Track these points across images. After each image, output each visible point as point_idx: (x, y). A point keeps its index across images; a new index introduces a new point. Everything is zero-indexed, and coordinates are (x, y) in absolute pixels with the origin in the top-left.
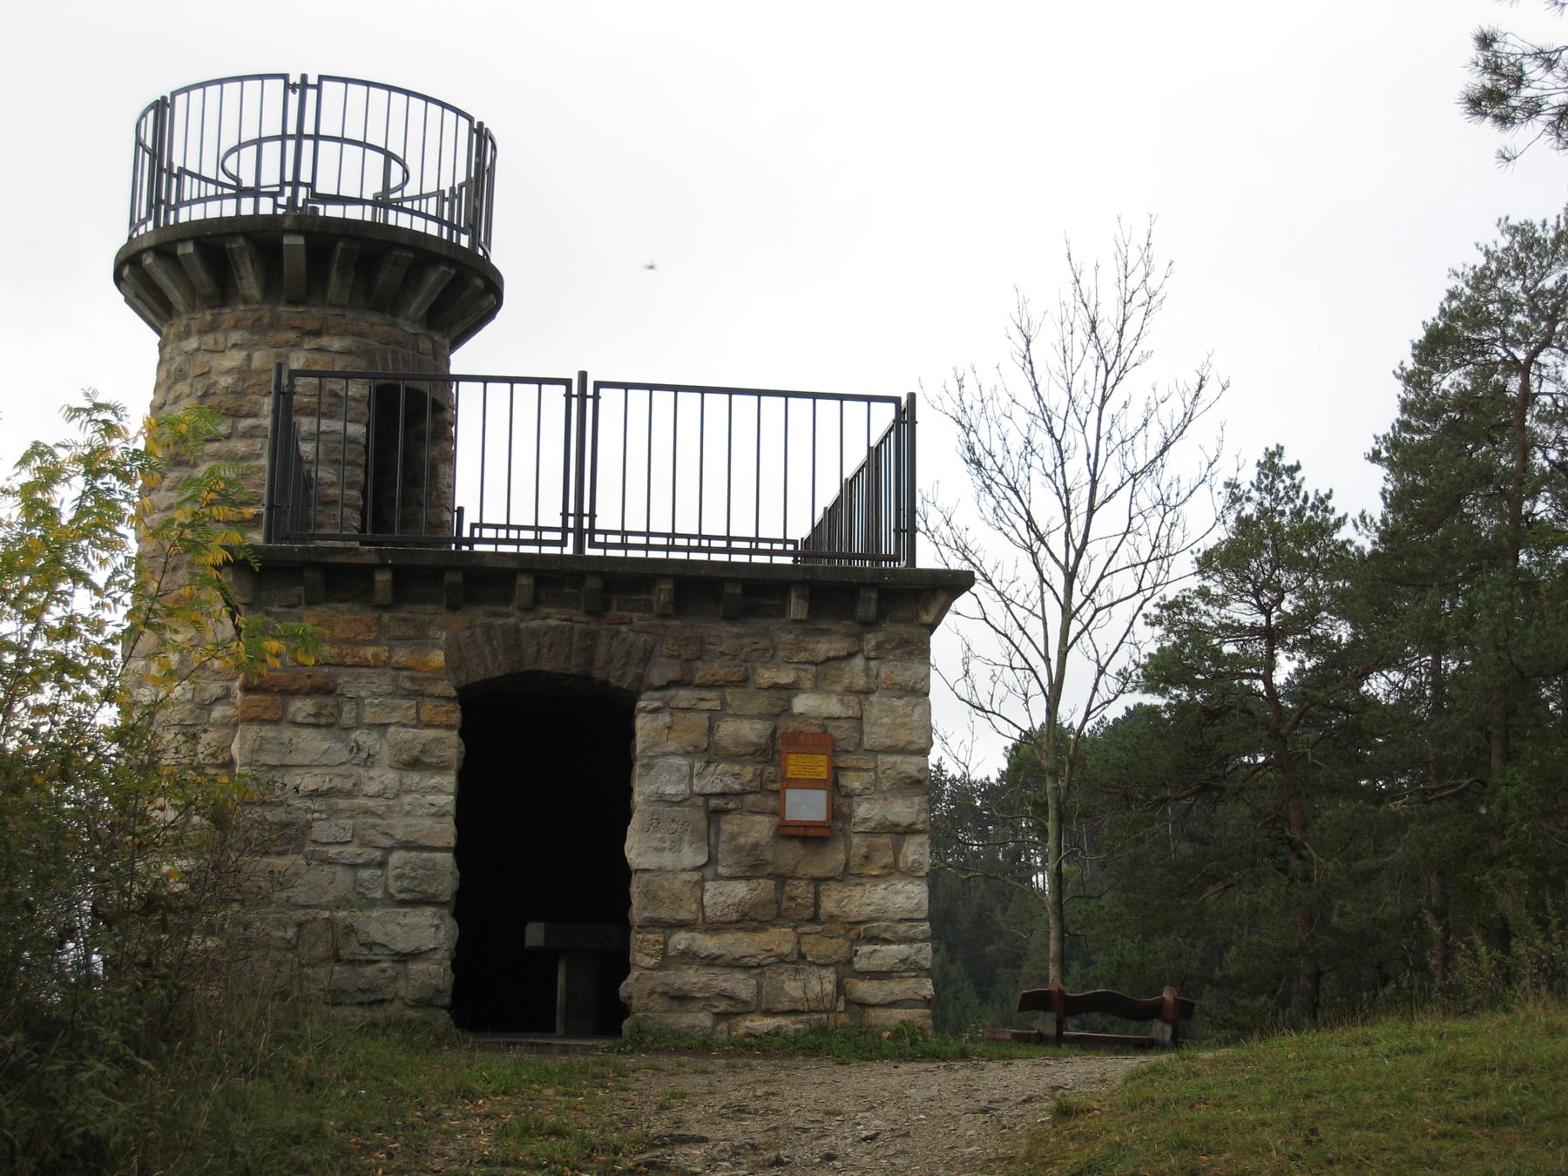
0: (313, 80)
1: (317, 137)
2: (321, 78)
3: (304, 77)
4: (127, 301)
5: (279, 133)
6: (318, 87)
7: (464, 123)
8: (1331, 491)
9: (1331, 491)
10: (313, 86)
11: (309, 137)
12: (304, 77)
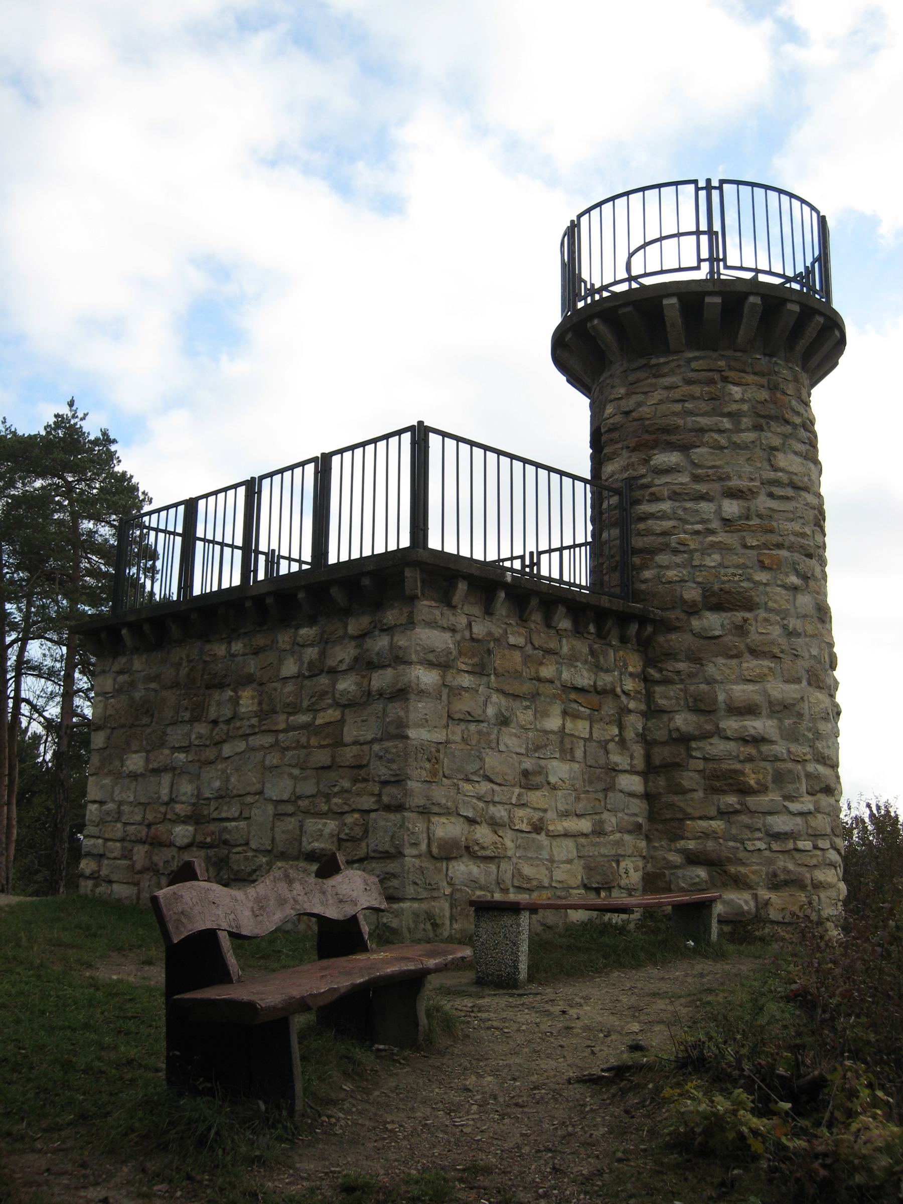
0: (715, 183)
1: (698, 233)
2: (722, 182)
3: (708, 181)
4: (568, 381)
5: (694, 229)
6: (720, 188)
7: (815, 215)
8: (4, 418)
9: (4, 418)
10: (715, 188)
11: (704, 233)
12: (708, 181)
